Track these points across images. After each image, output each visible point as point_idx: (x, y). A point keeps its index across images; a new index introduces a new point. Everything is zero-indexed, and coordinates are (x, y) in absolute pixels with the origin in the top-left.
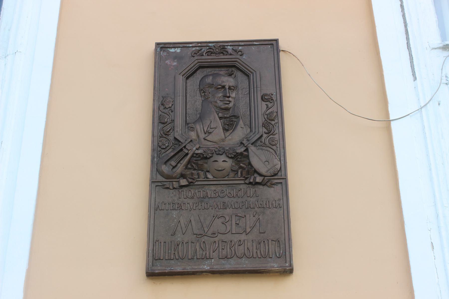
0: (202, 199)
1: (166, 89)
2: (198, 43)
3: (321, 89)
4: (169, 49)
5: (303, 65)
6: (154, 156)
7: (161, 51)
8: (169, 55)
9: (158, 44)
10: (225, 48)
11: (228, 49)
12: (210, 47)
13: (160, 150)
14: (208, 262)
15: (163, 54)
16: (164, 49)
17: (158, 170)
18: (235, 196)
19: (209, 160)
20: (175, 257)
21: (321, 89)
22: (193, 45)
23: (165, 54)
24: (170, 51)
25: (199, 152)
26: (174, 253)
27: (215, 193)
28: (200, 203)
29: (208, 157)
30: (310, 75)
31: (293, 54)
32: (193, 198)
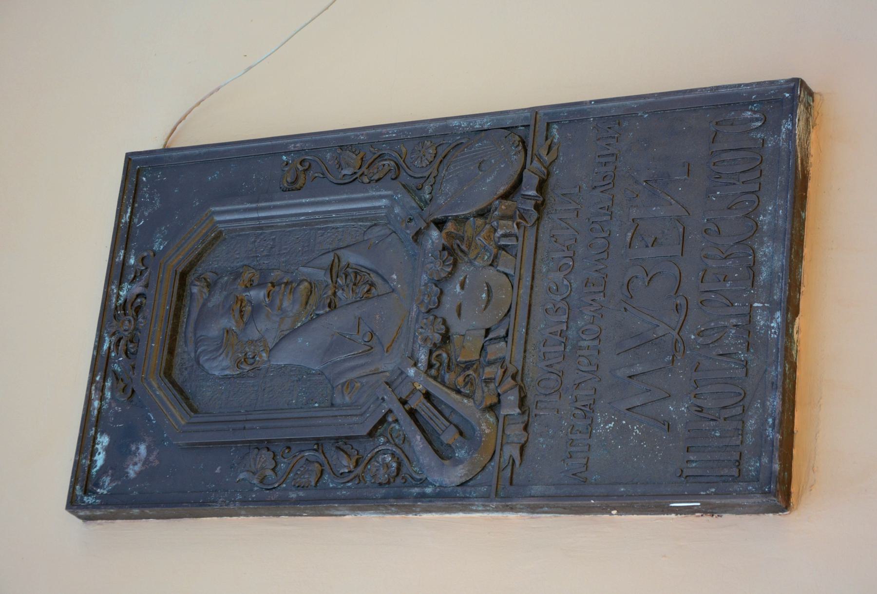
0: (569, 348)
1: (216, 471)
2: (92, 381)
3: (295, 34)
4: (95, 470)
5: (218, 89)
6: (418, 494)
7: (95, 493)
8: (112, 468)
9: (73, 504)
10: (120, 283)
11: (127, 296)
12: (112, 347)
13: (403, 478)
14: (760, 321)
15: (107, 485)
16: (90, 486)
17: (463, 480)
18: (570, 254)
19: (453, 330)
20: (738, 418)
21: (295, 34)
22: (95, 395)
23: (107, 480)
24: (102, 467)
25: (423, 357)
26: (723, 420)
27: (555, 310)
28: (580, 352)
29: (443, 332)
30: (250, 68)
31: (177, 120)
32: (561, 374)
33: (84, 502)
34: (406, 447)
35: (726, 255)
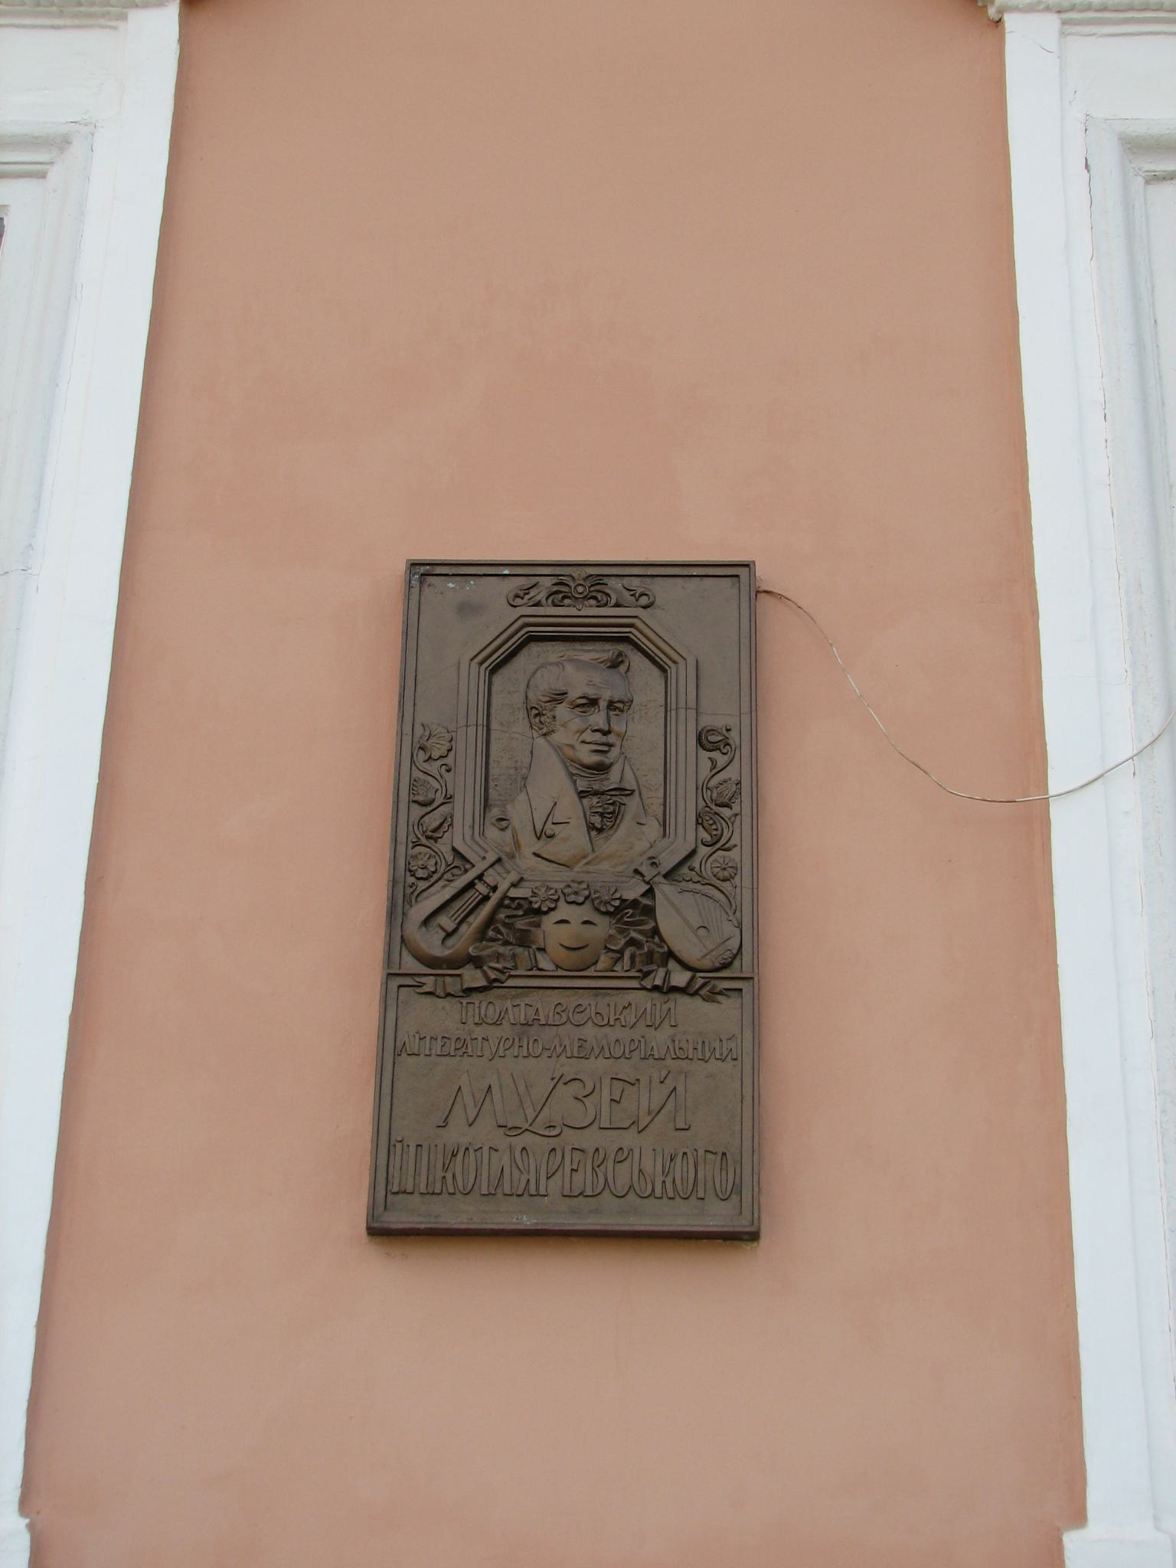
9: (414, 565)
33: (413, 576)
34: (441, 883)
35: (597, 1169)
